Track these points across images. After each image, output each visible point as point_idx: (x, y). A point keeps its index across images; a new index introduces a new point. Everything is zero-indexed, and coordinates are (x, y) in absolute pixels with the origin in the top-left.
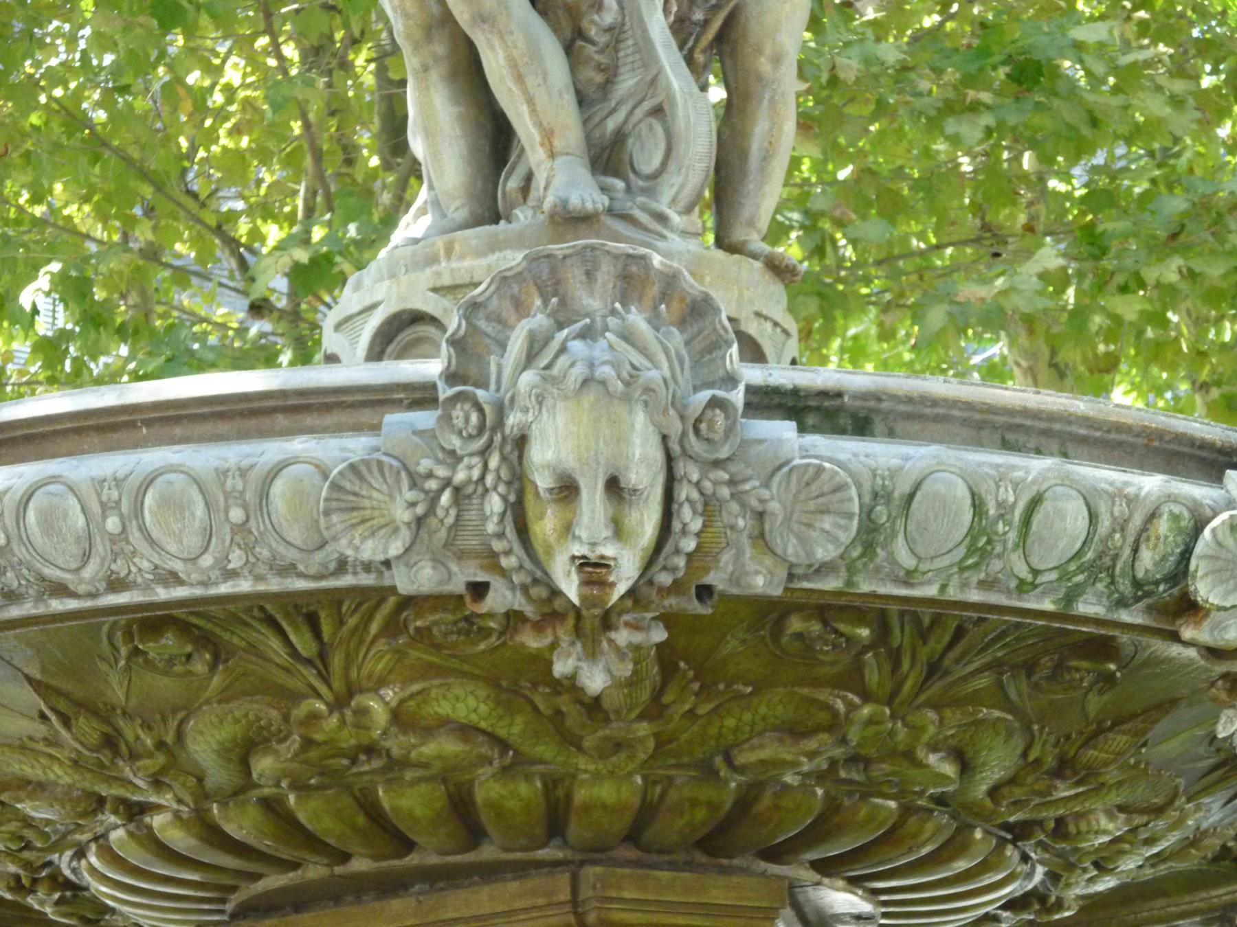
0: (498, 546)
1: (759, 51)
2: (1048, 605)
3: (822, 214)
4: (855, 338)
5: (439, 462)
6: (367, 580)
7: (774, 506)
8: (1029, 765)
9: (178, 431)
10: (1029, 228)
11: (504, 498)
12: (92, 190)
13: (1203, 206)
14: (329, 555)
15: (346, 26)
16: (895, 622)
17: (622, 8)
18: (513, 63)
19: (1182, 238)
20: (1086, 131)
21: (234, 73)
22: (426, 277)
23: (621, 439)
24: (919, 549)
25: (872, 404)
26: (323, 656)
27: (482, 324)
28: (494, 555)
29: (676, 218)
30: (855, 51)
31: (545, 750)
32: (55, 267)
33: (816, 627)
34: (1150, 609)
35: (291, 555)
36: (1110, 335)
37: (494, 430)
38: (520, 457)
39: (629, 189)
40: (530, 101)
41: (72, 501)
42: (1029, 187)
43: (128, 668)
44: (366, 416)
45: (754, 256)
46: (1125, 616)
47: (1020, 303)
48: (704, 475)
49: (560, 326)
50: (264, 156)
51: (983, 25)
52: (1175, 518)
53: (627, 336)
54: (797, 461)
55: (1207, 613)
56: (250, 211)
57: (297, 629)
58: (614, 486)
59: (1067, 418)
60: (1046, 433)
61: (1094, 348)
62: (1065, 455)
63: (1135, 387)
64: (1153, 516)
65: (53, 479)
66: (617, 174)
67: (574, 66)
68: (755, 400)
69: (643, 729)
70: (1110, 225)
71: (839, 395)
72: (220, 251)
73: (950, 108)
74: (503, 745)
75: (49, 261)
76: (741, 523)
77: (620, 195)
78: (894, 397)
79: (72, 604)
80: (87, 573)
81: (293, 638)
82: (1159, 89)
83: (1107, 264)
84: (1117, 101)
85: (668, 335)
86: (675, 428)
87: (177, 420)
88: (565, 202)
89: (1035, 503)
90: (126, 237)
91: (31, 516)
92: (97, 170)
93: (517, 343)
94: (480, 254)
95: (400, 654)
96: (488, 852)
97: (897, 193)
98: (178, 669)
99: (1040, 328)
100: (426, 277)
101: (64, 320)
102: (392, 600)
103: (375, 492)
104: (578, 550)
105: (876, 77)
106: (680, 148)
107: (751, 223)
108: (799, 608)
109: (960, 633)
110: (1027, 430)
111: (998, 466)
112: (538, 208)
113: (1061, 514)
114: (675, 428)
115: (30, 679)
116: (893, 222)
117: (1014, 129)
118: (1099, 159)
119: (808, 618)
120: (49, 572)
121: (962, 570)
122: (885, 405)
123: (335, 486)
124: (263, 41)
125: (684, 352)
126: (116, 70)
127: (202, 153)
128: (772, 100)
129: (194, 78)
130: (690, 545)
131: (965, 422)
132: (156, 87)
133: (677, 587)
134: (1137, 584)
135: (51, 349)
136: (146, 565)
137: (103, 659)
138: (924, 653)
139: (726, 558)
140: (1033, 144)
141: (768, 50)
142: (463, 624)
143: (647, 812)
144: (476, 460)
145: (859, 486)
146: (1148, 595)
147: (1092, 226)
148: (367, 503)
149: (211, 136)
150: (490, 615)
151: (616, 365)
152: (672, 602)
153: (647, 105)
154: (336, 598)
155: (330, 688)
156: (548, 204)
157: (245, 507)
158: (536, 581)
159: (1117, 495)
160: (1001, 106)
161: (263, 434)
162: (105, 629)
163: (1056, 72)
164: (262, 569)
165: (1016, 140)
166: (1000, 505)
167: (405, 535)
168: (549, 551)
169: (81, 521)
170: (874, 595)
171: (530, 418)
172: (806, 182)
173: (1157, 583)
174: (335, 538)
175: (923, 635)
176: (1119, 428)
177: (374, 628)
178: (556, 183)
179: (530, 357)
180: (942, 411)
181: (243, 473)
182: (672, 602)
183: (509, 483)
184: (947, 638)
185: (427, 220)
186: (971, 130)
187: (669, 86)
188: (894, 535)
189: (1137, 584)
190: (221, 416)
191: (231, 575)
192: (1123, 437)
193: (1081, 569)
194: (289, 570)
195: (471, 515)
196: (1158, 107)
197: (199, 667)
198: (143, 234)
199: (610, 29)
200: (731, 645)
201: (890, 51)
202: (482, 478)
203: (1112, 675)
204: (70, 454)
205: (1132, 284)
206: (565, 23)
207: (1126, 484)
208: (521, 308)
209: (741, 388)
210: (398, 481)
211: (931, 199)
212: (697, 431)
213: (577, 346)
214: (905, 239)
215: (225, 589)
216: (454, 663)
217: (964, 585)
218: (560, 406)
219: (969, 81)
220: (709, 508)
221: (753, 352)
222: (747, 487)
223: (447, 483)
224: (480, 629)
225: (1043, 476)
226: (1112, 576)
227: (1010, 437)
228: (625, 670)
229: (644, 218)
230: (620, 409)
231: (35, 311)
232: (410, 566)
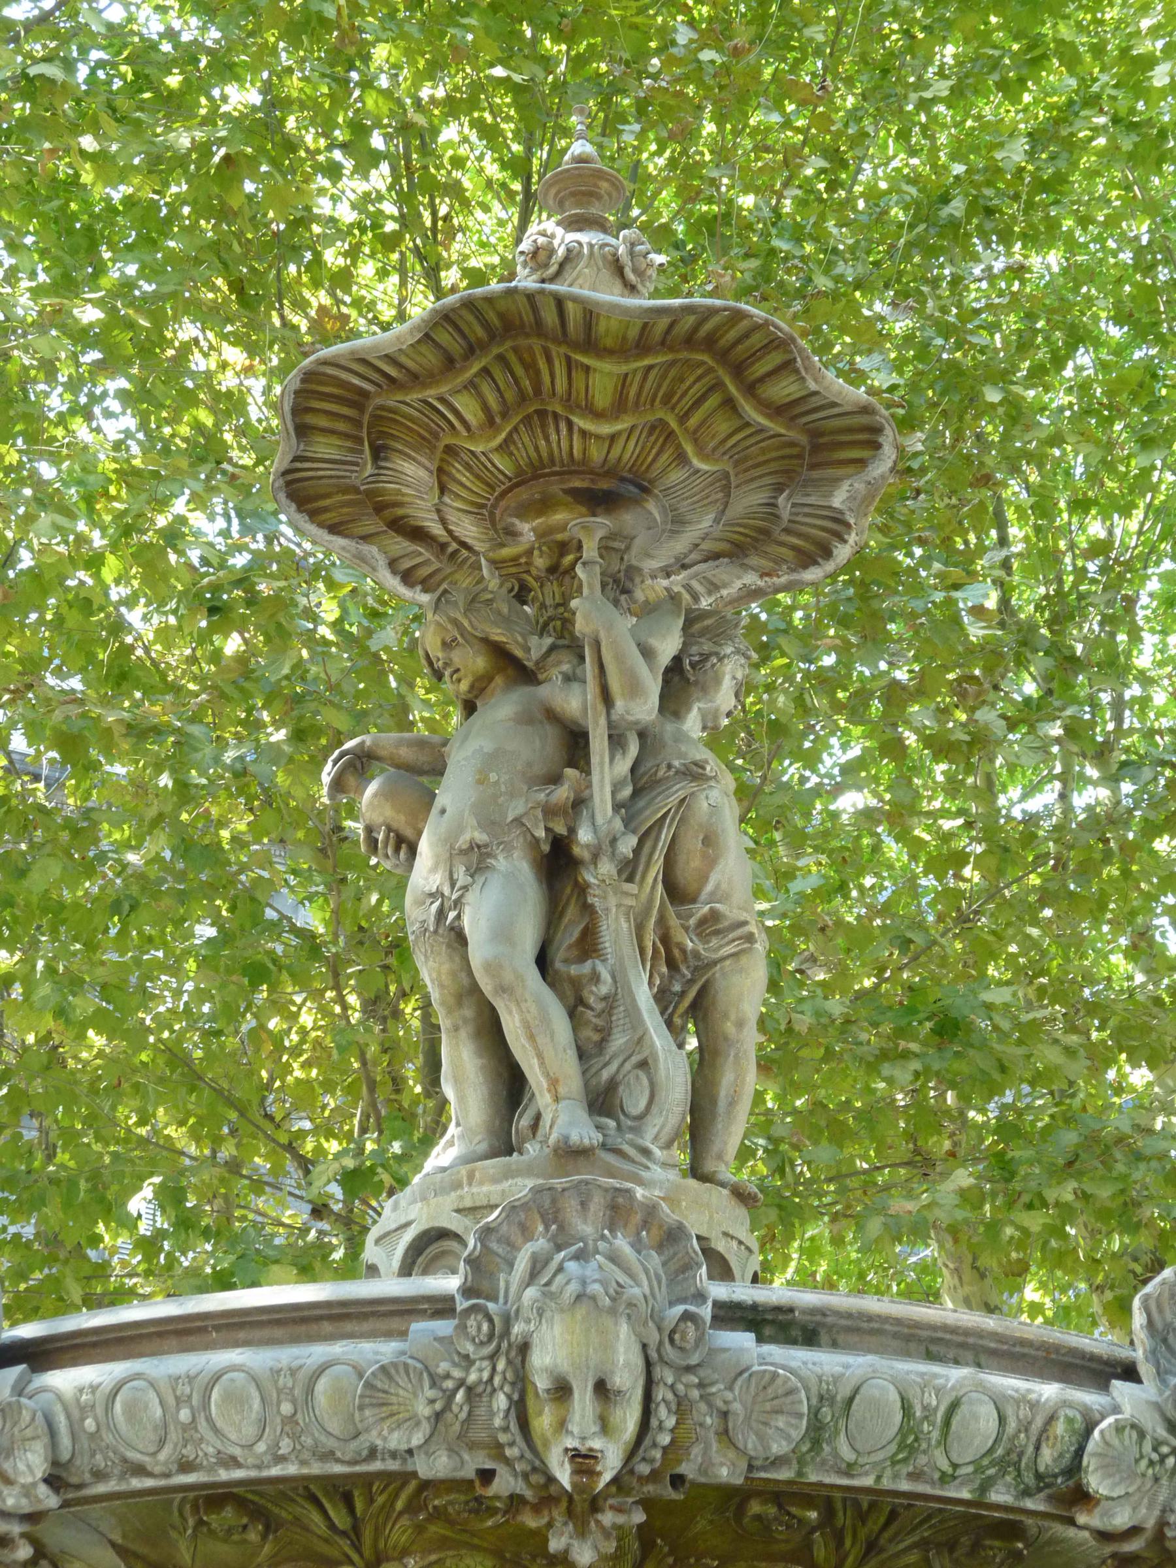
0: (503, 1438)
1: (726, 1016)
2: (965, 1495)
3: (781, 1140)
4: (812, 1239)
5: (455, 1365)
6: (393, 1466)
7: (737, 1407)
9: (242, 1335)
10: (952, 1154)
11: (509, 1397)
12: (189, 1114)
13: (1092, 1139)
14: (363, 1443)
15: (399, 981)
16: (839, 1506)
17: (615, 981)
18: (527, 1026)
19: (1077, 1165)
20: (996, 1076)
21: (307, 1019)
22: (450, 1200)
23: (607, 1346)
24: (858, 1446)
25: (818, 1318)
26: (356, 1528)
27: (494, 1246)
28: (500, 1446)
29: (657, 1152)
30: (806, 1007)
32: (157, 1180)
33: (772, 1510)
34: (1050, 1498)
35: (331, 1443)
36: (1020, 1245)
37: (501, 1337)
38: (523, 1361)
39: (619, 1127)
40: (540, 1056)
41: (152, 1395)
42: (952, 1120)
43: (195, 1535)
44: (395, 1323)
45: (722, 1185)
46: (1029, 1504)
47: (941, 1215)
48: (677, 1379)
49: (559, 1248)
50: (328, 1086)
51: (911, 988)
52: (1070, 1421)
53: (614, 1258)
54: (756, 1368)
55: (1098, 1502)
56: (316, 1131)
57: (334, 1506)
58: (602, 1388)
59: (980, 1333)
60: (963, 1346)
61: (1008, 1255)
62: (979, 1365)
63: (1043, 1285)
64: (1051, 1419)
65: (137, 1376)
66: (609, 1115)
67: (575, 1029)
68: (722, 1313)
70: (1017, 1153)
71: (791, 1310)
72: (290, 1164)
73: (884, 1056)
75: (152, 1174)
76: (709, 1420)
77: (612, 1132)
78: (838, 1313)
79: (149, 1483)
80: (162, 1456)
81: (332, 1513)
82: (1056, 1041)
83: (1016, 1185)
84: (1021, 1051)
85: (647, 1257)
86: (653, 1337)
87: (241, 1326)
88: (566, 1139)
89: (954, 1406)
90: (214, 1153)
91: (118, 1407)
92: (193, 1098)
93: (522, 1263)
94: (495, 1180)
95: (420, 1529)
97: (844, 1123)
98: (236, 1537)
99: (963, 1238)
100: (450, 1200)
101: (162, 1223)
102: (412, 1486)
103: (402, 1390)
104: (570, 1443)
105: (825, 1027)
106: (661, 1095)
107: (720, 1157)
108: (758, 1494)
109: (893, 1515)
110: (947, 1343)
111: (922, 1375)
112: (544, 1142)
113: (975, 1417)
114: (653, 1337)
115: (113, 1545)
116: (841, 1147)
117: (937, 1074)
118: (1009, 1097)
119: (765, 1502)
120: (131, 1455)
121: (894, 1463)
122: (829, 1320)
123: (369, 1385)
124: (330, 994)
125: (661, 1272)
126: (212, 1018)
127: (278, 1084)
128: (736, 1056)
129: (274, 1024)
130: (665, 1439)
131: (895, 1336)
132: (244, 1028)
133: (654, 1476)
134: (1039, 1477)
135: (149, 1245)
136: (211, 1450)
137: (173, 1527)
138: (863, 1533)
139: (696, 1451)
140: (953, 1086)
141: (733, 1017)
142: (473, 1504)
144: (486, 1363)
145: (807, 1390)
146: (1048, 1486)
147: (1002, 1153)
148: (394, 1399)
149: (287, 1069)
150: (497, 1497)
151: (604, 1283)
152: (650, 1489)
153: (635, 1059)
154: (367, 1480)
155: (361, 1556)
156: (552, 1140)
157: (294, 1402)
158: (535, 1469)
159: (1020, 1400)
160: (925, 1054)
161: (312, 1339)
162: (176, 1503)
163: (970, 1028)
164: (306, 1455)
165: (940, 1082)
166: (925, 1408)
167: (426, 1428)
168: (546, 1444)
169: (159, 1412)
170: (821, 1485)
171: (532, 1327)
172: (769, 1112)
173: (1055, 1476)
174: (367, 1430)
175: (862, 1517)
176: (1023, 1342)
177: (399, 1505)
178: (559, 1121)
179: (533, 1275)
180: (876, 1325)
181: (293, 1372)
182: (650, 1489)
183: (513, 1384)
184: (882, 1520)
186: (903, 1074)
187: (653, 1044)
188: (837, 1432)
189: (1039, 1477)
190: (278, 1323)
191: (280, 1459)
192: (1026, 1350)
193: (992, 1464)
194: (328, 1456)
195: (481, 1411)
196: (1053, 1055)
197: (253, 1536)
198: (227, 1151)
199: (605, 998)
200: (701, 1524)
201: (836, 1006)
202: (491, 1379)
203: (1020, 1552)
204: (153, 1354)
205: (1037, 1203)
206: (569, 993)
207: (1029, 1391)
208: (527, 1233)
209: (710, 1304)
210: (421, 1380)
211: (871, 1129)
212: (672, 1341)
213: (572, 1266)
214: (852, 1159)
215: (275, 1471)
216: (465, 1537)
217: (896, 1476)
218: (557, 1318)
219: (901, 1032)
220: (682, 1407)
221: (722, 1270)
222: (714, 1390)
223: (461, 1383)
224: (488, 1508)
225: (960, 1383)
226: (1018, 1470)
227: (934, 1348)
228: (610, 1547)
229: (631, 1152)
230: (608, 1321)
231: (140, 1216)
232: (428, 1455)
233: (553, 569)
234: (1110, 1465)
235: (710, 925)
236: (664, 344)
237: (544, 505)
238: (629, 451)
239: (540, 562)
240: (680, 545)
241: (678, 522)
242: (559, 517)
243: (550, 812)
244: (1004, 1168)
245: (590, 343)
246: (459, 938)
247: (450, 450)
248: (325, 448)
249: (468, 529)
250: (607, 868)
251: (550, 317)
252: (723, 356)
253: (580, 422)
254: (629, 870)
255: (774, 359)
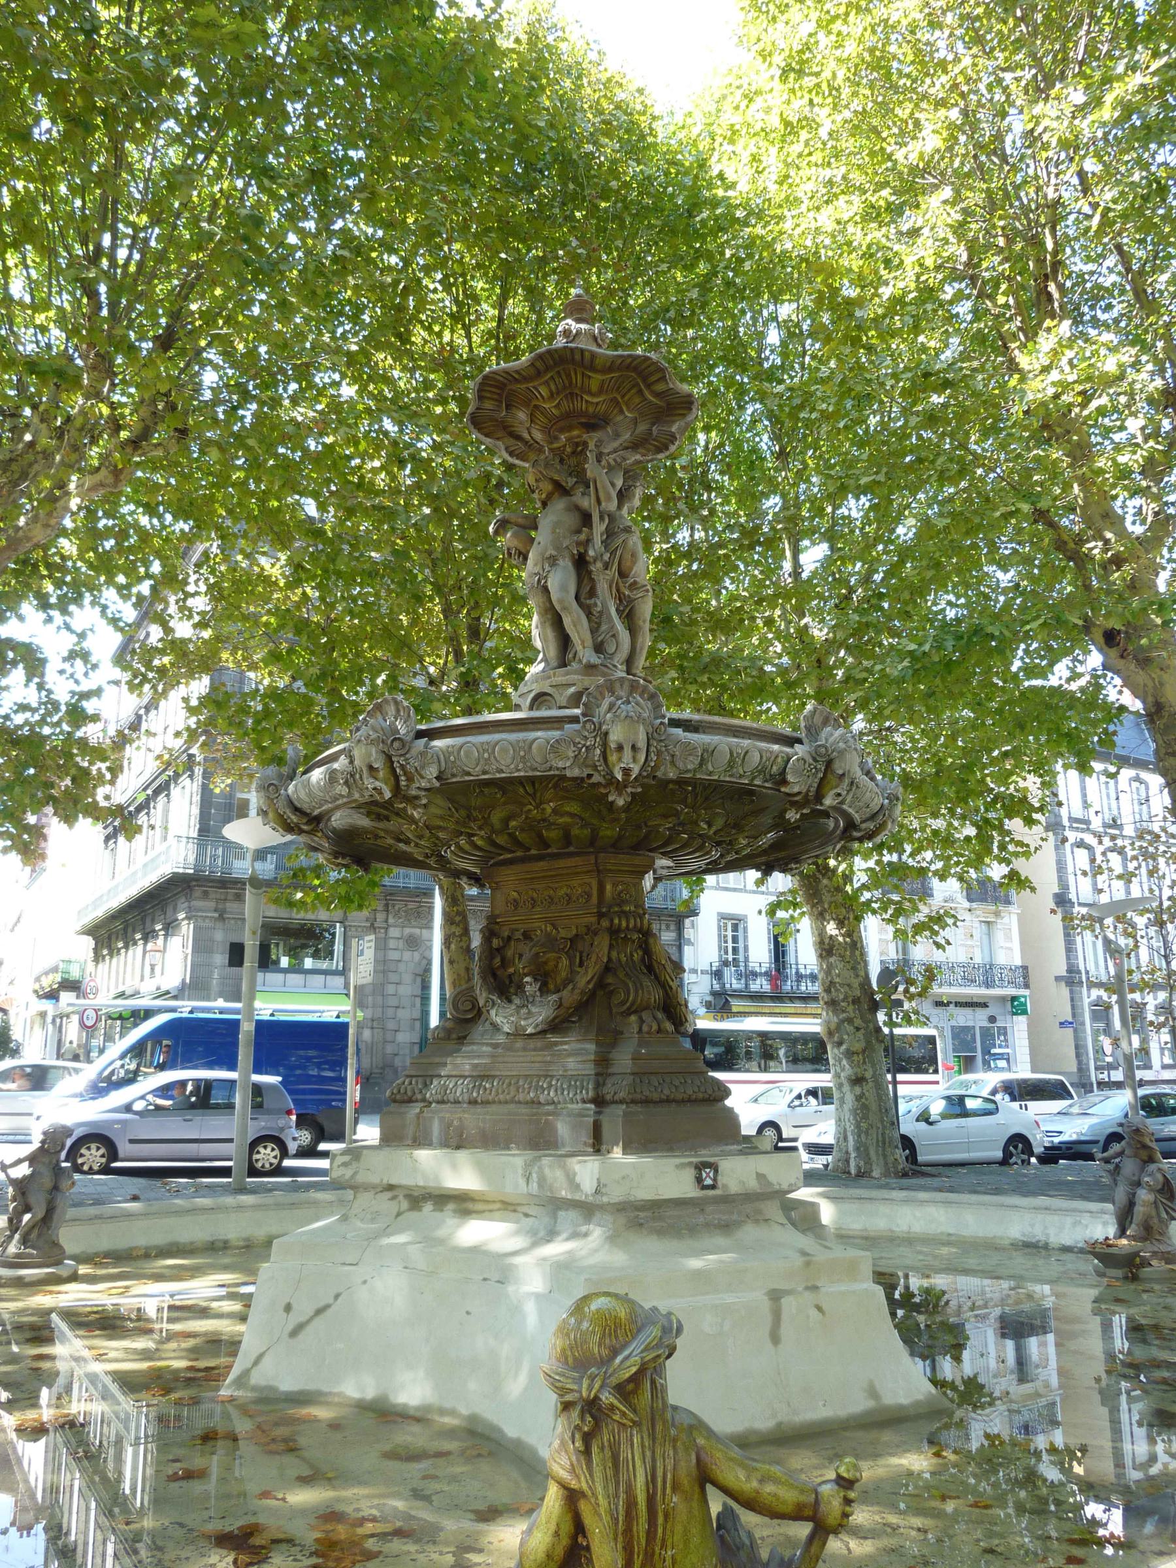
8: (726, 825)
23: (636, 733)
31: (595, 821)
58: (634, 748)
69: (623, 816)
74: (582, 819)
96: (572, 849)
133: (647, 777)
143: (620, 837)
179: (610, 709)
185: (542, 665)
194: (536, 769)
233: (573, 453)
234: (795, 772)
235: (634, 586)
236: (619, 369)
237: (570, 428)
238: (603, 408)
239: (569, 450)
240: (616, 444)
241: (617, 435)
242: (575, 433)
243: (578, 544)
244: (681, 668)
245: (592, 368)
246: (546, 590)
247: (536, 407)
248: (488, 405)
249: (538, 436)
250: (599, 565)
251: (578, 357)
252: (640, 374)
253: (585, 397)
254: (607, 566)
255: (659, 375)
